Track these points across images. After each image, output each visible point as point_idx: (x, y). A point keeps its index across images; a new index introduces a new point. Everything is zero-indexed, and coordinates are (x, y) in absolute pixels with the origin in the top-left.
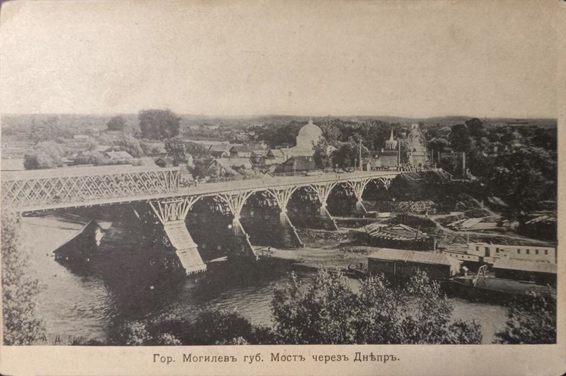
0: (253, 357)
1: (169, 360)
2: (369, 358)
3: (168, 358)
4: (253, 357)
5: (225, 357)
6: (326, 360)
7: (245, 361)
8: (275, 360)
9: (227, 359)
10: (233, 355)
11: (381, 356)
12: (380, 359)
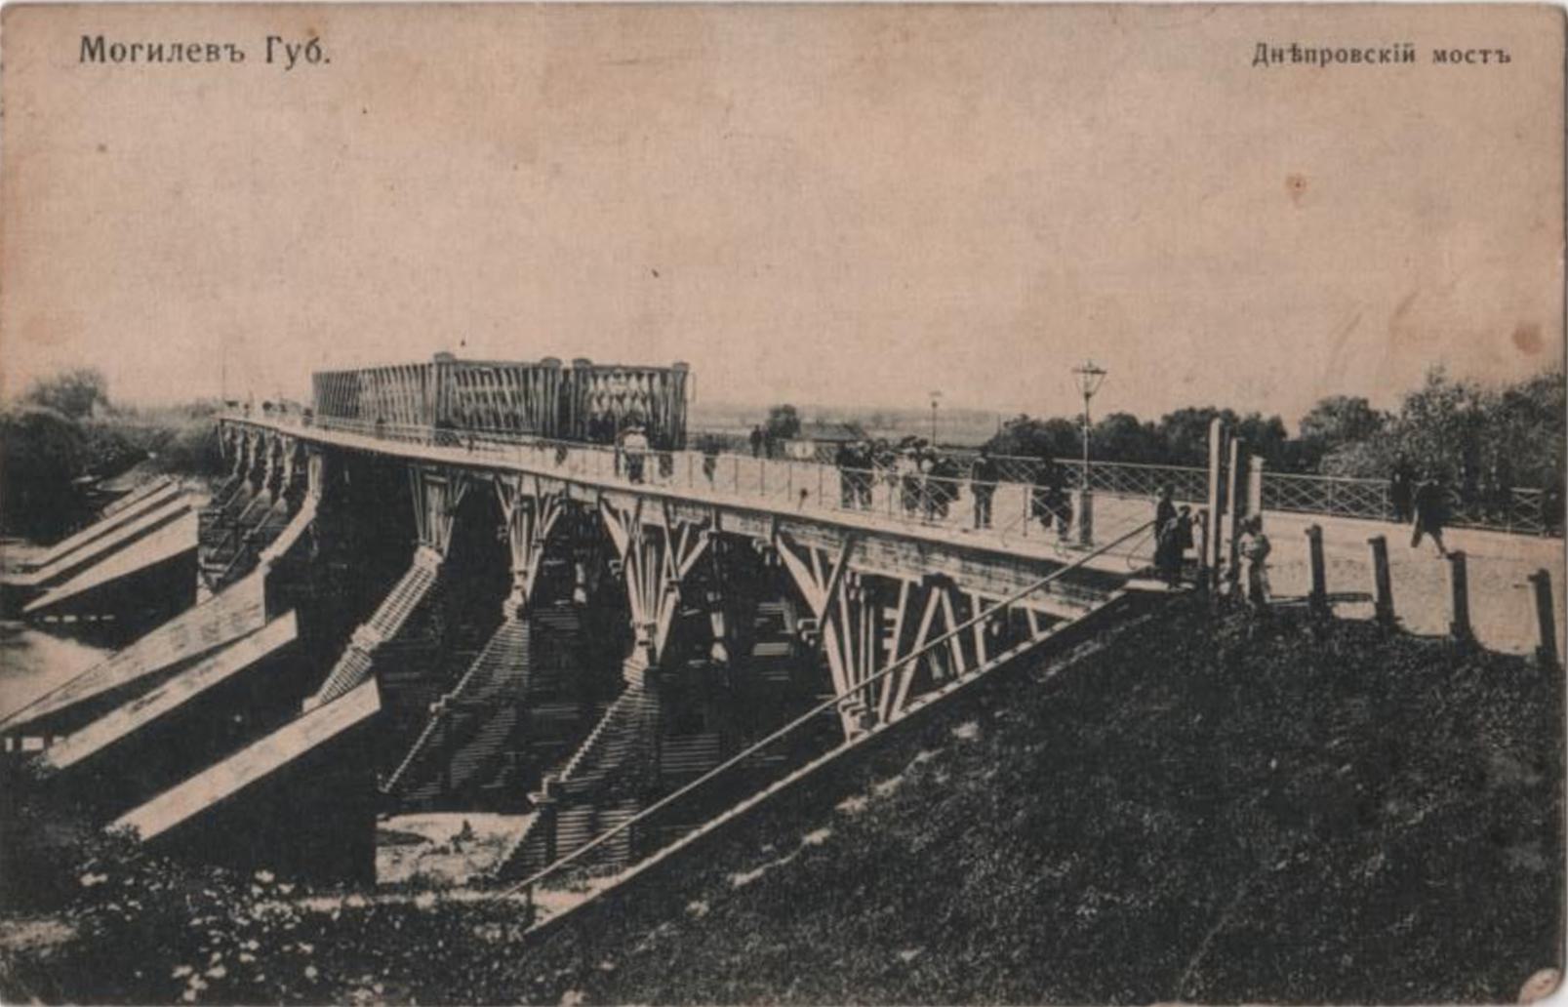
2: (1288, 56)
10: (232, 42)
11: (1314, 52)
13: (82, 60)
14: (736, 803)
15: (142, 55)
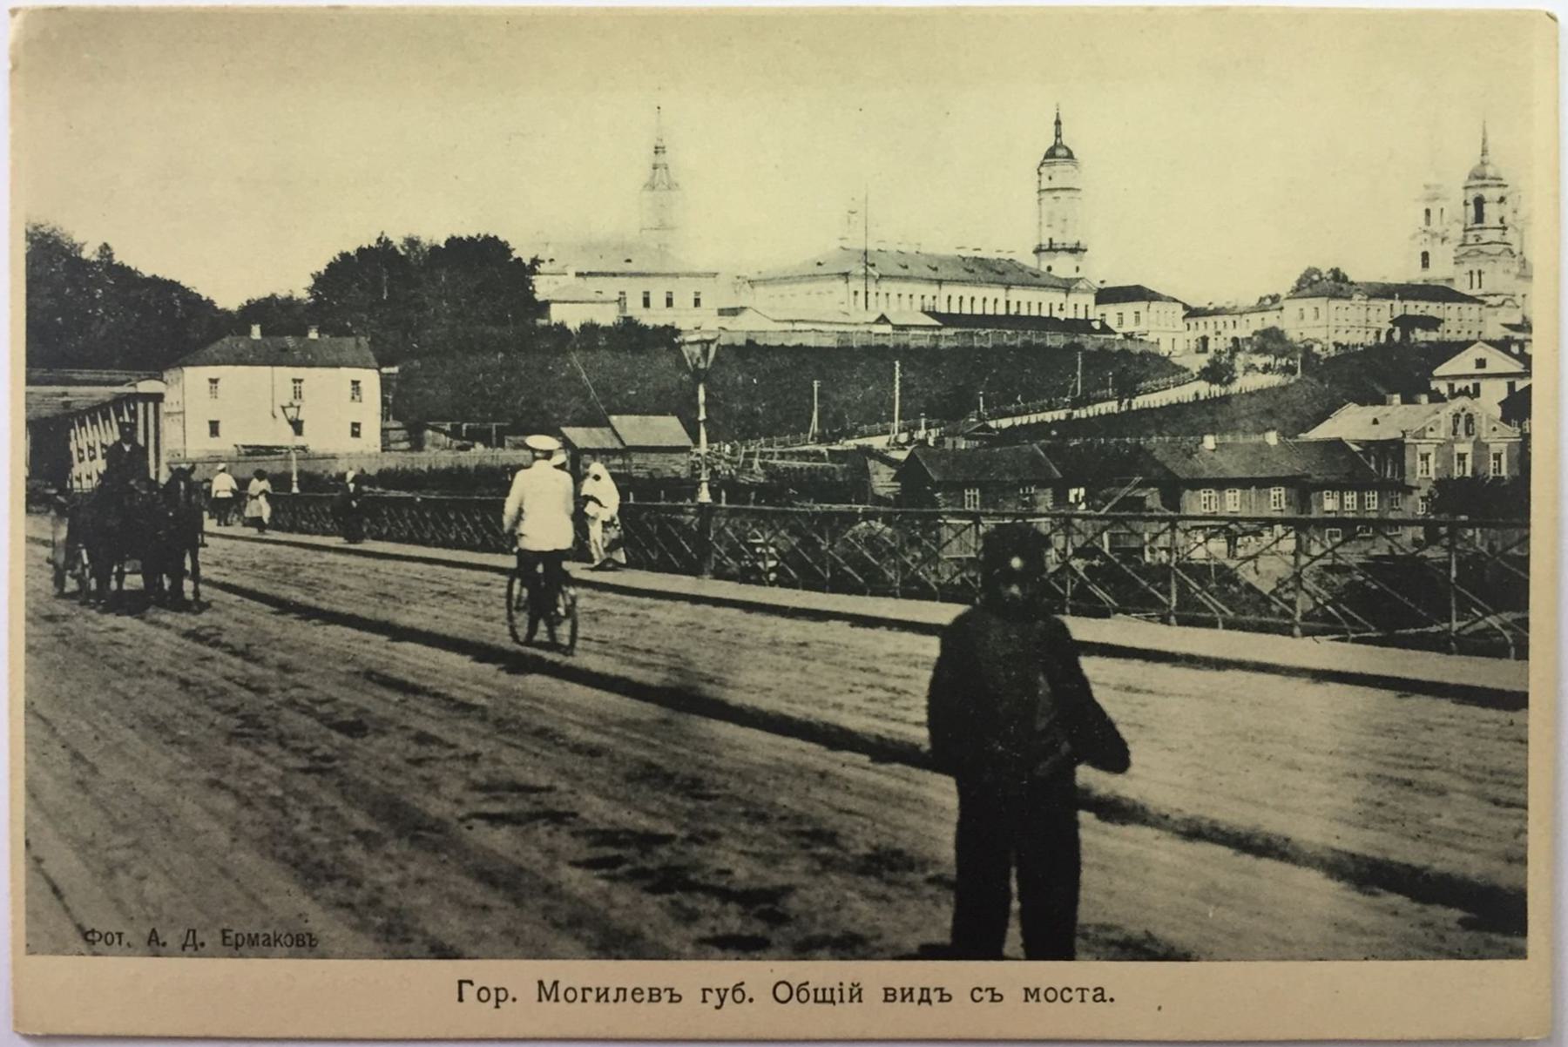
0: (726, 990)
1: (499, 996)
3: (497, 990)
4: (726, 990)
5: (651, 989)
6: (498, 1000)
7: (704, 1001)
8: (548, 998)
9: (655, 995)
12: (828, 993)
13: (1026, 1000)
14: (1008, 889)
15: (591, 996)
